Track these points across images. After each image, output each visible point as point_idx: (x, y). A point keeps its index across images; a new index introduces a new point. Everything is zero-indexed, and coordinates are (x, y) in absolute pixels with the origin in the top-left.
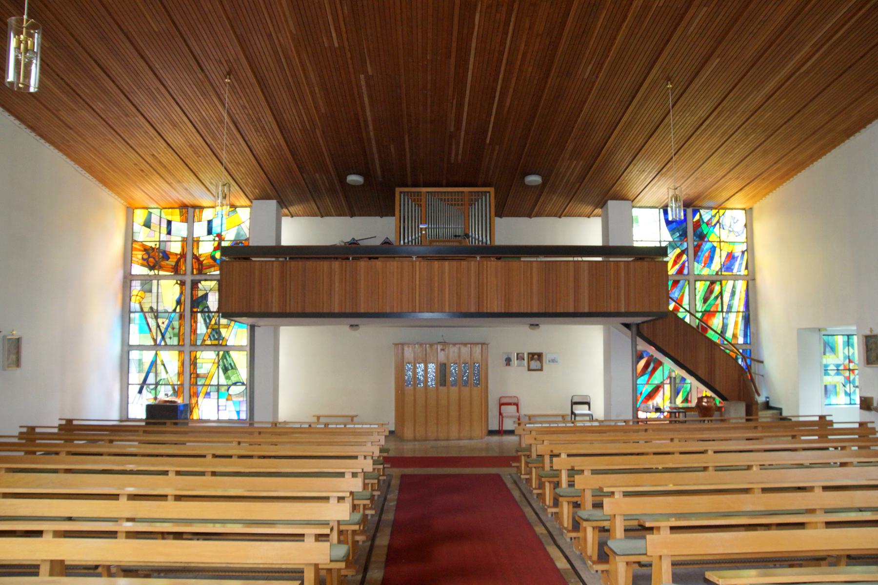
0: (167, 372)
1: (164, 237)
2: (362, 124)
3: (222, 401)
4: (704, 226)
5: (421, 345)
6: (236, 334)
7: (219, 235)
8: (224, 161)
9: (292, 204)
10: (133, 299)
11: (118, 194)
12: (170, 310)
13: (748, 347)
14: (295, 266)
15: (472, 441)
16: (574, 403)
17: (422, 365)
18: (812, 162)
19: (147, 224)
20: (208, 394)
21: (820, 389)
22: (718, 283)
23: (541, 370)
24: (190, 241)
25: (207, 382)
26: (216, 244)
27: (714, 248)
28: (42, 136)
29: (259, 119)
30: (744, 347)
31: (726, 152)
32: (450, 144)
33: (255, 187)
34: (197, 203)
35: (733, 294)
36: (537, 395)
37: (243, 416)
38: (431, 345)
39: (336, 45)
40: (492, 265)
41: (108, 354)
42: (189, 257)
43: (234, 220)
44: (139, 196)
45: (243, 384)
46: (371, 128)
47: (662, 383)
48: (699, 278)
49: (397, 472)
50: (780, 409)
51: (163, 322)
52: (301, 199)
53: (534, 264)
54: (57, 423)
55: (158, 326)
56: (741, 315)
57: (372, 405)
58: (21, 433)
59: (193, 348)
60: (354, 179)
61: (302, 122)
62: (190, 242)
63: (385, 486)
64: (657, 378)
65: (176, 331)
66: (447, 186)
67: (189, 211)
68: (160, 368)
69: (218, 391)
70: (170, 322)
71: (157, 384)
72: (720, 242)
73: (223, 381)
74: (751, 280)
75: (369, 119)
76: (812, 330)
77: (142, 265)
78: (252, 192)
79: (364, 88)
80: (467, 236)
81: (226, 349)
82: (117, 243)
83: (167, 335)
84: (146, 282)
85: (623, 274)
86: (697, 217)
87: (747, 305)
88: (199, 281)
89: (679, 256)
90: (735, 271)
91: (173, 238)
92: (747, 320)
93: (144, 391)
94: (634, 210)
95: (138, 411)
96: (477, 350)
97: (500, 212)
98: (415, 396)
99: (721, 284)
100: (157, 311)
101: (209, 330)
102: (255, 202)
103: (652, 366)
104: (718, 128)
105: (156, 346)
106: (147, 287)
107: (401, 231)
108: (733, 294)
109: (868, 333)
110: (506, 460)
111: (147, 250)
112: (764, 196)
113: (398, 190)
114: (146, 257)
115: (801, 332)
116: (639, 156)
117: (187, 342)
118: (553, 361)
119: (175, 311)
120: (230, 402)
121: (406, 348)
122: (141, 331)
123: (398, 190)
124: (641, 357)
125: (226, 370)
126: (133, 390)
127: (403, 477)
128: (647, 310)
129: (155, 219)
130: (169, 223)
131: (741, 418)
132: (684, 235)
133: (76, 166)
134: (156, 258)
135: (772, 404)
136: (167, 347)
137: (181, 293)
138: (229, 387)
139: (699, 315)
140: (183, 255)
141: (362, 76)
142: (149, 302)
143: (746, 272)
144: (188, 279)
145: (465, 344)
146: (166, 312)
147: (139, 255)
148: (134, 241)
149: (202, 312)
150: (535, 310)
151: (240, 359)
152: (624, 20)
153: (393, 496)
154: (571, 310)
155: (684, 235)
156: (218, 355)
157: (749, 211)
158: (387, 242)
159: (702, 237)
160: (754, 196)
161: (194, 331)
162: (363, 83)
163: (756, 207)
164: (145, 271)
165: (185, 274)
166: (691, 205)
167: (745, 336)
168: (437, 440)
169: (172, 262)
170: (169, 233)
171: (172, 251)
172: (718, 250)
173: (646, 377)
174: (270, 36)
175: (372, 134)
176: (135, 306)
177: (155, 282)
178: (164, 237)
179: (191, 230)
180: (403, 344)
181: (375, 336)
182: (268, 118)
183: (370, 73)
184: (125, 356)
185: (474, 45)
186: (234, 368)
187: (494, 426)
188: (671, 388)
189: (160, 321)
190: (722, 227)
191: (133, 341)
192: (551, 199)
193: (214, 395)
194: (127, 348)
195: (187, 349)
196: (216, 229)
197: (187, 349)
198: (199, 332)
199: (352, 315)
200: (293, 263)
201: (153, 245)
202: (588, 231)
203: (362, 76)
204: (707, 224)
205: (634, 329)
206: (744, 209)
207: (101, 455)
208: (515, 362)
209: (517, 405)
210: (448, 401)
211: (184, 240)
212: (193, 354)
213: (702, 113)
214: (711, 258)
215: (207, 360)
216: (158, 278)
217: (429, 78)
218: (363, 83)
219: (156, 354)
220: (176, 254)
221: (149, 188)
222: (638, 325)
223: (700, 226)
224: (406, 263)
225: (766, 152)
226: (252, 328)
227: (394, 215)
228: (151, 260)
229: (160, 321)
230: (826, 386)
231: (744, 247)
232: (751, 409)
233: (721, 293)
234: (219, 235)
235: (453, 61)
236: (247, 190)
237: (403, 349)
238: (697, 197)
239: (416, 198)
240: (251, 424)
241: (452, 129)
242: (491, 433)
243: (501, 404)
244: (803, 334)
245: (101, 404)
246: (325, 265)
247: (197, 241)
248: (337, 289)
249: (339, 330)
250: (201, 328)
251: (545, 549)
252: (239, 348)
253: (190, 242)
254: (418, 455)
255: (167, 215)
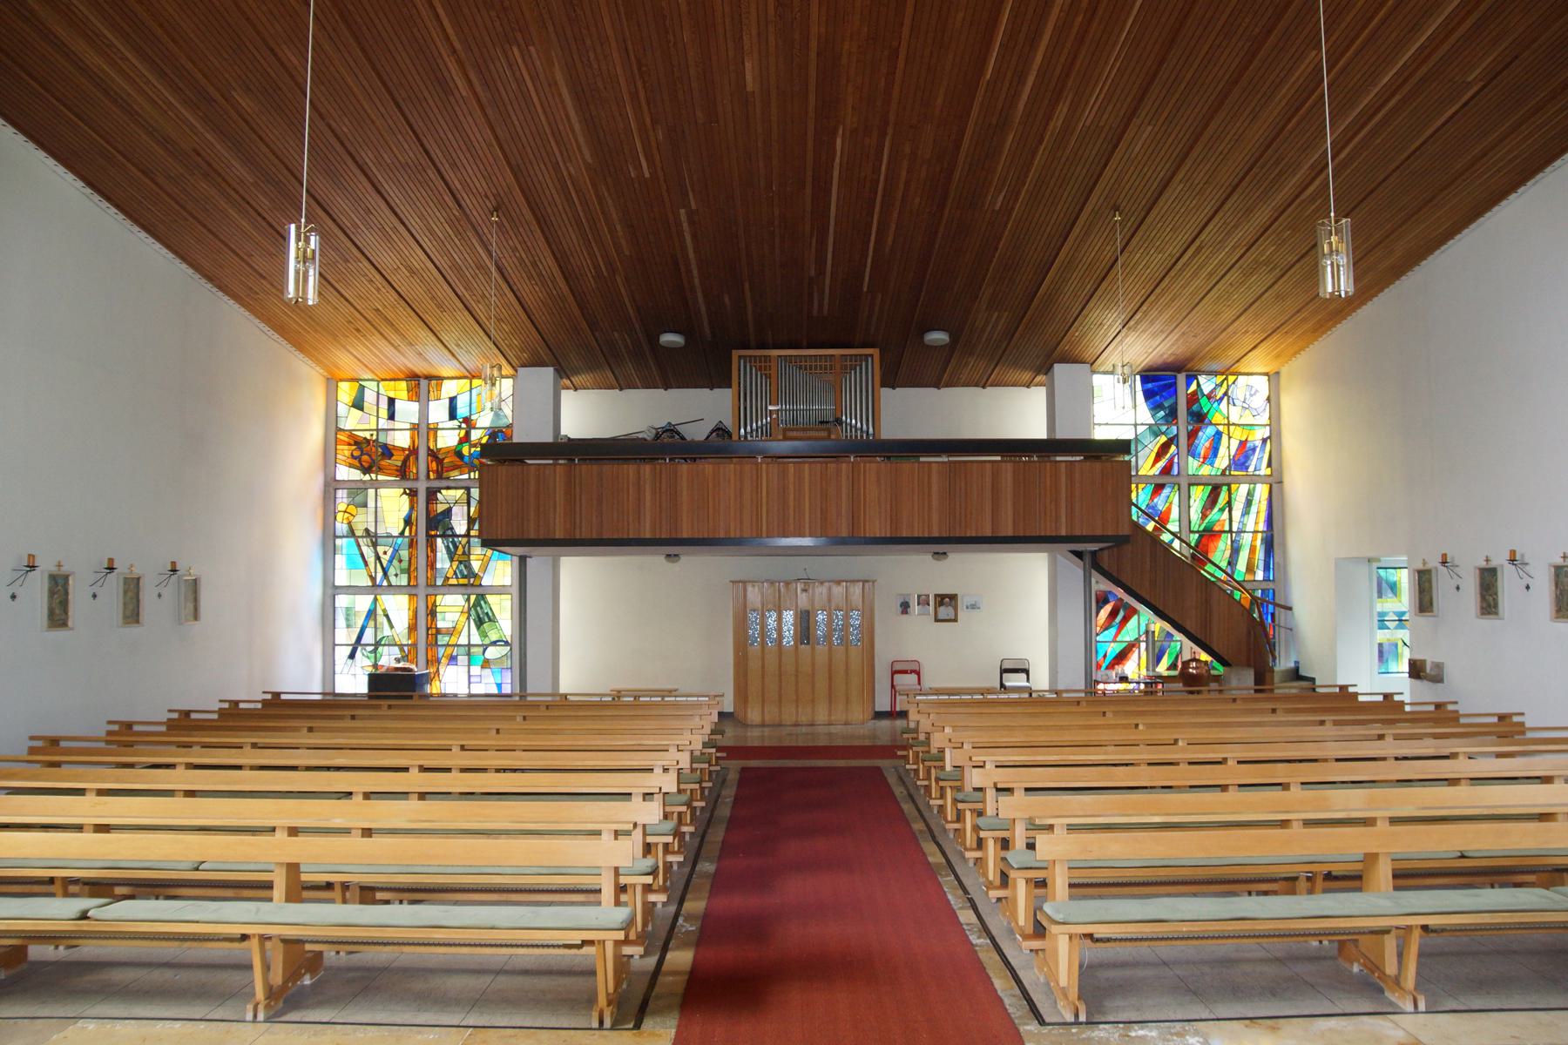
0: (392, 627)
1: (384, 423)
2: (683, 268)
3: (476, 670)
4: (1204, 401)
5: (772, 583)
6: (499, 570)
7: (467, 420)
8: (493, 333)
9: (577, 372)
10: (340, 516)
11: (318, 361)
12: (396, 533)
13: (1271, 586)
14: (586, 471)
15: (839, 721)
16: (1004, 671)
17: (774, 615)
18: (1354, 310)
19: (358, 404)
20: (453, 659)
21: (1355, 643)
22: (1225, 488)
23: (955, 620)
24: (423, 430)
25: (453, 640)
26: (463, 433)
27: (1219, 434)
28: (222, 288)
29: (534, 264)
30: (1265, 585)
31: (1219, 298)
32: (811, 295)
33: (522, 351)
34: (434, 372)
35: (1249, 503)
36: (948, 657)
37: (507, 689)
38: (787, 584)
39: (647, 175)
40: (874, 468)
41: (310, 602)
42: (423, 453)
43: (484, 397)
44: (344, 361)
45: (507, 643)
46: (695, 272)
47: (1138, 640)
48: (1196, 481)
49: (735, 765)
50: (1313, 680)
51: (385, 551)
52: (591, 365)
53: (935, 468)
54: (164, 716)
55: (378, 558)
56: (1259, 536)
57: (699, 667)
58: (109, 733)
59: (431, 590)
60: (669, 338)
61: (597, 267)
62: (425, 429)
63: (720, 780)
64: (1131, 631)
65: (405, 565)
66: (809, 347)
67: (421, 383)
68: (381, 619)
69: (469, 654)
70: (396, 551)
71: (377, 644)
72: (1228, 425)
73: (476, 639)
74: (1276, 483)
75: (693, 262)
76: (1357, 560)
77: (351, 466)
78: (518, 358)
79: (685, 225)
80: (838, 421)
81: (479, 591)
82: (314, 434)
83: (392, 571)
84: (358, 493)
85: (1063, 479)
86: (1193, 387)
87: (1270, 521)
88: (439, 490)
89: (1164, 448)
90: (1251, 469)
91: (397, 425)
92: (1269, 545)
93: (358, 654)
94: (1095, 377)
95: (353, 680)
96: (857, 590)
97: (892, 379)
98: (763, 659)
99: (1229, 490)
100: (376, 536)
101: (455, 564)
102: (521, 370)
103: (1121, 614)
104: (1201, 267)
105: (375, 588)
106: (359, 499)
107: (741, 415)
108: (1249, 503)
109: (1420, 566)
110: (889, 751)
111: (358, 443)
112: (1294, 355)
113: (736, 353)
114: (356, 454)
115: (1339, 563)
116: (1091, 304)
117: (422, 580)
118: (974, 607)
119: (402, 534)
120: (487, 671)
121: (750, 588)
122: (351, 566)
123: (736, 353)
124: (1106, 602)
125: (480, 623)
126: (342, 653)
127: (744, 770)
128: (1099, 532)
129: (370, 397)
130: (391, 401)
131: (1247, 689)
132: (1172, 415)
133: (262, 325)
134: (372, 455)
135: (1303, 672)
136: (396, 589)
137: (412, 508)
138: (485, 647)
139: (1194, 538)
140: (413, 451)
141: (682, 211)
142: (363, 520)
143: (1268, 471)
144: (422, 486)
145: (839, 582)
146: (390, 536)
147: (345, 451)
148: (339, 430)
149: (443, 536)
150: (936, 534)
151: (502, 608)
152: (1040, 142)
153: (729, 793)
154: (988, 533)
155: (1172, 415)
156: (468, 600)
157: (1273, 377)
158: (720, 430)
159: (1200, 418)
160: (1278, 356)
161: (431, 564)
162: (683, 218)
163: (1284, 371)
164: (356, 475)
165: (417, 479)
166: (1185, 367)
167: (1267, 568)
168: (796, 725)
169: (397, 461)
170: (391, 417)
171: (397, 444)
172: (1225, 438)
173: (1113, 631)
174: (556, 166)
175: (697, 281)
176: (341, 527)
177: (371, 492)
178: (384, 423)
179: (424, 413)
180: (744, 582)
181: (698, 567)
182: (548, 263)
183: (694, 206)
184: (329, 602)
185: (836, 173)
186: (492, 619)
187: (883, 704)
188: (1142, 646)
189: (380, 549)
190: (1231, 402)
191: (341, 579)
192: (967, 364)
193: (462, 659)
194: (332, 590)
195: (422, 591)
196: (462, 411)
197: (422, 591)
198: (439, 566)
199: (671, 542)
200: (584, 468)
201: (367, 435)
202: (1022, 413)
203: (682, 211)
204: (1209, 397)
205: (1088, 558)
206: (1266, 374)
207: (239, 767)
208: (915, 608)
209: (918, 673)
210: (813, 664)
211: (415, 428)
212: (431, 600)
213: (1174, 249)
214: (1214, 449)
215: (451, 608)
216: (377, 485)
217: (777, 212)
218: (683, 218)
219: (376, 600)
220: (403, 449)
221: (361, 350)
222: (1094, 553)
223: (1197, 400)
224: (748, 467)
225: (1279, 297)
226: (523, 560)
227: (730, 386)
228: (365, 458)
229: (380, 549)
230: (1380, 645)
231: (1266, 432)
232: (1263, 678)
233: (1229, 504)
234: (467, 420)
235: (808, 190)
236: (510, 355)
237: (745, 590)
238: (1190, 359)
239: (763, 365)
240: (523, 696)
241: (813, 273)
242: (879, 715)
243: (894, 673)
244: (1343, 566)
245: (299, 676)
246: (630, 470)
247: (434, 430)
248: (648, 504)
249: (651, 562)
250: (443, 562)
251: (919, 845)
252: (500, 590)
253: (425, 429)
254: (767, 743)
255: (388, 389)
